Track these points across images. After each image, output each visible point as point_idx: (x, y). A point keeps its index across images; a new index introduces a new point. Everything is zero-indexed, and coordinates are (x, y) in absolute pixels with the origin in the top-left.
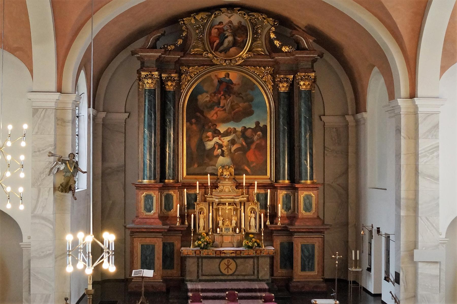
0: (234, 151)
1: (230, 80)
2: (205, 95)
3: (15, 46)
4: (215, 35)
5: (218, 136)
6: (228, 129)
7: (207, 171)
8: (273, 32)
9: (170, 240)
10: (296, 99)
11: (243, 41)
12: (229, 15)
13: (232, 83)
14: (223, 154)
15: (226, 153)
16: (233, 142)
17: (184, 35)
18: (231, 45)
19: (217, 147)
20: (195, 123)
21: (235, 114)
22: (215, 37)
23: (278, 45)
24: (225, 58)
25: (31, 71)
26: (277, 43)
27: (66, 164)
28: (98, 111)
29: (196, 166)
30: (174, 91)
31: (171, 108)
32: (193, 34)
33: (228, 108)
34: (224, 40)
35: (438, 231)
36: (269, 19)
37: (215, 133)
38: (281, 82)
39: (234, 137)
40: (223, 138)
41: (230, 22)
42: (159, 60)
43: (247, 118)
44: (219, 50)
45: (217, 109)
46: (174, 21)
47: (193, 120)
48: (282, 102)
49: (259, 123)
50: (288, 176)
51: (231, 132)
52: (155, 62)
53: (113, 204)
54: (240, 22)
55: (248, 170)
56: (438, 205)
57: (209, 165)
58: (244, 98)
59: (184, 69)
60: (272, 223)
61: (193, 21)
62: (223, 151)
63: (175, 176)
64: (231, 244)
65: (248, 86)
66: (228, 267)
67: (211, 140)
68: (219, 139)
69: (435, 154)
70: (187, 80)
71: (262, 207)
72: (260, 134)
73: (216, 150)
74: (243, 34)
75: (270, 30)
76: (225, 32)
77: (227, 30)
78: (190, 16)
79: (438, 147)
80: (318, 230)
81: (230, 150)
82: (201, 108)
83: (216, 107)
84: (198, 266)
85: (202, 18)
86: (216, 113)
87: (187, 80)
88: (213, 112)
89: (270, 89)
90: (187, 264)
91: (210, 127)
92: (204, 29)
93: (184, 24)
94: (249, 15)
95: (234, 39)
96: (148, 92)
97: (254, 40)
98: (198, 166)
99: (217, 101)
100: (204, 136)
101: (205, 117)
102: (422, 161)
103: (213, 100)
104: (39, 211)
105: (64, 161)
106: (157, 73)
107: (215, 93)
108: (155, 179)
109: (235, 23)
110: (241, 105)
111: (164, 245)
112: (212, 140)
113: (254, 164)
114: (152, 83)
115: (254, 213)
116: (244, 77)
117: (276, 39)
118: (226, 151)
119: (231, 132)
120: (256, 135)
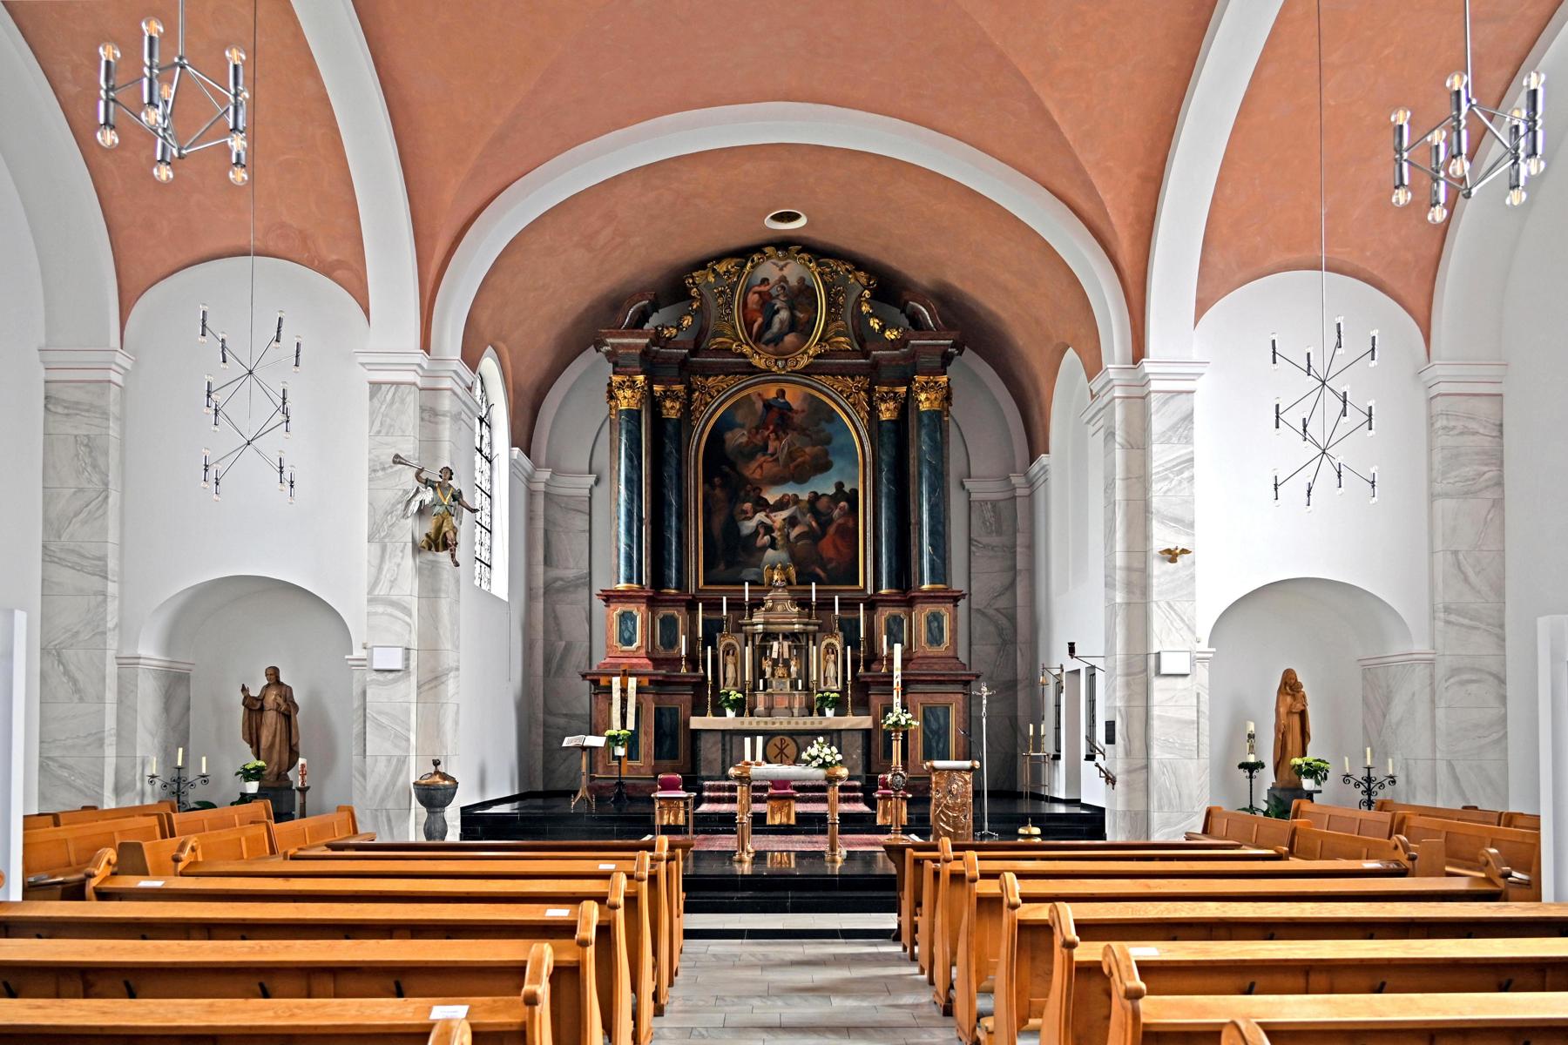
3: (334, 257)
8: (867, 301)
9: (668, 702)
10: (912, 434)
13: (790, 409)
15: (780, 542)
16: (792, 522)
18: (786, 329)
19: (762, 531)
25: (367, 312)
26: (875, 324)
27: (434, 489)
28: (536, 466)
29: (722, 567)
30: (679, 420)
32: (713, 305)
33: (782, 457)
35: (1192, 630)
38: (883, 400)
41: (783, 279)
42: (645, 352)
46: (674, 288)
50: (888, 541)
53: (568, 648)
54: (802, 280)
55: (822, 574)
56: (1193, 578)
60: (867, 668)
61: (711, 279)
62: (773, 539)
63: (681, 585)
66: (782, 750)
69: (1186, 474)
71: (846, 643)
78: (705, 268)
79: (1192, 460)
84: (724, 750)
85: (728, 271)
86: (761, 466)
88: (753, 465)
91: (747, 494)
94: (819, 265)
95: (793, 316)
101: (740, 475)
102: (1158, 489)
104: (382, 590)
105: (428, 483)
106: (641, 377)
107: (757, 428)
108: (640, 581)
109: (793, 281)
110: (807, 450)
111: (659, 712)
116: (813, 397)
117: (872, 315)
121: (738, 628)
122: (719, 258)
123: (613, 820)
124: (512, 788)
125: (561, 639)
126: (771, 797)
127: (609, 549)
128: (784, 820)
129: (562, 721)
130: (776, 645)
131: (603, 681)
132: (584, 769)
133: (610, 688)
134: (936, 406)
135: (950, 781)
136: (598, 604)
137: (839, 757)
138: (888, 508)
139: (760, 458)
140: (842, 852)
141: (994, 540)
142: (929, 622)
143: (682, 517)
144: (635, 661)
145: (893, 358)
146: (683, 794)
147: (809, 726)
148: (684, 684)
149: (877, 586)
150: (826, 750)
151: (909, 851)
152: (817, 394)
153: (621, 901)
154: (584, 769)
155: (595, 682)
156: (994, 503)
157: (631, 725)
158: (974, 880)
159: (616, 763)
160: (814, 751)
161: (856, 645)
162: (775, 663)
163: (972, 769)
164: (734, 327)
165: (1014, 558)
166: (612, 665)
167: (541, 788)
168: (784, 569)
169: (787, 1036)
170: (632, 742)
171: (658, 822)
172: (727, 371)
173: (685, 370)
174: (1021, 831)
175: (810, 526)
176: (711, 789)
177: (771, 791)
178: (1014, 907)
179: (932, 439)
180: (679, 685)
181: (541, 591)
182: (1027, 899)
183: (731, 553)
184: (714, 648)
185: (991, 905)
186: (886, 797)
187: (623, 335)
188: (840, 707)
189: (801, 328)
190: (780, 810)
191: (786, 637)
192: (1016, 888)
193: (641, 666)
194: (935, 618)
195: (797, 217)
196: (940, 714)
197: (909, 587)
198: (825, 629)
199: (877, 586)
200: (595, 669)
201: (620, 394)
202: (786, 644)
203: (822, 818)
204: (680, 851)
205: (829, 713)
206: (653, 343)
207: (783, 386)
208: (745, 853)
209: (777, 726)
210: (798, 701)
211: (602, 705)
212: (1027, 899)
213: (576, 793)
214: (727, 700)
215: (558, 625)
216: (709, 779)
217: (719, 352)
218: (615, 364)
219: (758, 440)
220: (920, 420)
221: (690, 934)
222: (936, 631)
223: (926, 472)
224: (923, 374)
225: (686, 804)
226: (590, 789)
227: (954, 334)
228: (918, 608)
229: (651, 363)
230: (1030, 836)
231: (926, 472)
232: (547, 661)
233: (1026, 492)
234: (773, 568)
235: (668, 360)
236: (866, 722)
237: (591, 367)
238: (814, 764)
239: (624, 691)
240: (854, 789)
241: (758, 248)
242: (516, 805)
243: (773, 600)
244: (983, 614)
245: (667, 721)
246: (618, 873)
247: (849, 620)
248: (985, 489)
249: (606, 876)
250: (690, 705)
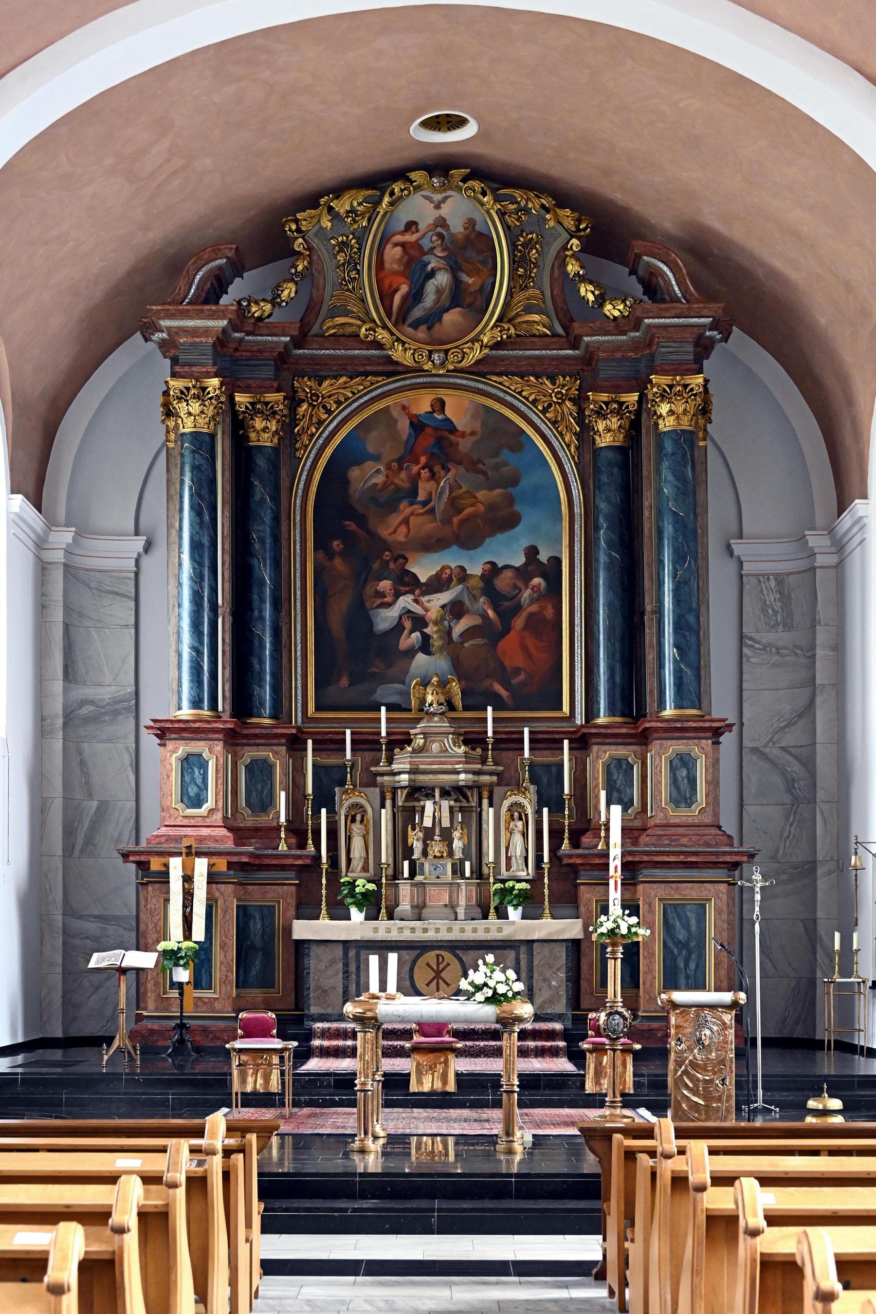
1: (448, 420)
2: (370, 466)
4: (395, 267)
6: (443, 568)
9: (257, 896)
10: (648, 467)
12: (438, 197)
13: (453, 430)
14: (425, 647)
15: (437, 642)
16: (456, 609)
17: (300, 268)
18: (445, 300)
19: (408, 624)
20: (342, 554)
21: (462, 522)
22: (396, 273)
23: (591, 298)
26: (587, 292)
28: (51, 523)
29: (344, 682)
30: (276, 450)
32: (329, 264)
33: (440, 505)
36: (560, 212)
37: (404, 584)
38: (600, 414)
39: (461, 593)
40: (426, 598)
41: (441, 222)
42: (222, 341)
43: (500, 537)
44: (409, 321)
46: (268, 237)
47: (337, 545)
48: (604, 478)
49: (538, 552)
50: (608, 639)
52: (209, 351)
53: (103, 808)
55: (504, 693)
57: (384, 680)
59: (306, 385)
60: (575, 843)
61: (326, 223)
62: (426, 638)
64: (448, 911)
65: (503, 436)
66: (438, 973)
67: (389, 605)
68: (416, 601)
70: (314, 420)
71: (541, 802)
72: (540, 584)
73: (406, 632)
75: (565, 248)
76: (426, 258)
77: (433, 248)
78: (315, 205)
80: (713, 859)
81: (449, 632)
82: (360, 508)
83: (403, 504)
84: (346, 972)
85: (352, 211)
86: (406, 521)
87: (314, 420)
88: (395, 519)
89: (568, 446)
90: (312, 966)
92: (359, 249)
93: (298, 230)
94: (497, 199)
95: (456, 282)
98: (350, 685)
99: (406, 485)
100: (369, 591)
101: (374, 536)
103: (396, 481)
106: (215, 382)
107: (400, 461)
108: (213, 706)
109: (457, 226)
111: (244, 913)
113: (522, 677)
114: (202, 412)
115: (520, 819)
117: (583, 279)
118: (435, 636)
120: (527, 587)
121: (371, 780)
122: (338, 190)
123: (169, 1083)
124: (14, 1032)
125: (90, 796)
126: (417, 1049)
127: (167, 656)
128: (438, 1086)
129: (92, 927)
130: (429, 806)
131: (155, 864)
132: (122, 1004)
133: (166, 874)
134: (686, 424)
135: (700, 1025)
136: (149, 740)
137: (519, 987)
138: (610, 587)
139: (405, 509)
140: (523, 1137)
141: (781, 637)
142: (673, 770)
143: (280, 603)
144: (205, 832)
145: (619, 347)
146: (277, 1044)
147: (481, 936)
148: (283, 868)
149: (591, 712)
150: (498, 976)
151: (617, 1137)
152: (496, 406)
153: (132, 1222)
154: (122, 1004)
155: (143, 866)
156: (780, 579)
157: (199, 933)
158: (701, 1189)
159: (175, 994)
160: (477, 977)
161: (556, 807)
162: (429, 834)
163: (735, 1004)
164: (363, 300)
165: (812, 667)
166: (169, 839)
167: (59, 1034)
168: (443, 684)
170: (201, 961)
171: (236, 1087)
172: (355, 370)
174: (812, 1104)
175: (484, 616)
176: (325, 1034)
177: (417, 1038)
178: (755, 1233)
179: (680, 477)
180: (276, 870)
181: (60, 722)
182: (774, 1219)
183: (358, 659)
184: (331, 812)
185: (723, 1227)
186: (599, 1049)
187: (185, 315)
188: (531, 904)
189: (474, 302)
190: (432, 1068)
191: (445, 793)
192: (756, 1201)
193: (216, 840)
194: (685, 762)
195: (461, 122)
196: (692, 916)
198: (507, 781)
199: (591, 712)
200: (143, 844)
201: (182, 408)
202: (445, 804)
203: (493, 1081)
204: (253, 1138)
205: (514, 914)
206: (234, 326)
207: (442, 393)
208: (372, 1139)
209: (431, 935)
210: (465, 895)
211: (154, 903)
212: (774, 1219)
213: (109, 1040)
214: (352, 894)
215: (86, 775)
216: (322, 1018)
217: (338, 339)
218: (175, 361)
220: (660, 447)
221: (271, 1267)
223: (668, 529)
224: (665, 373)
225: (282, 1058)
226: (133, 1035)
227: (717, 308)
228: (655, 746)
229: (231, 359)
230: (826, 1113)
231: (668, 529)
232: (69, 831)
233: (833, 560)
234: (425, 683)
235: (258, 353)
236: (571, 928)
237: (137, 363)
238: (480, 997)
239: (188, 879)
240: (551, 1035)
241: (401, 174)
242: (20, 1059)
243: (426, 735)
244: (764, 756)
245: (256, 926)
246: (128, 1178)
247: (548, 766)
248: (764, 556)
249: (111, 1179)
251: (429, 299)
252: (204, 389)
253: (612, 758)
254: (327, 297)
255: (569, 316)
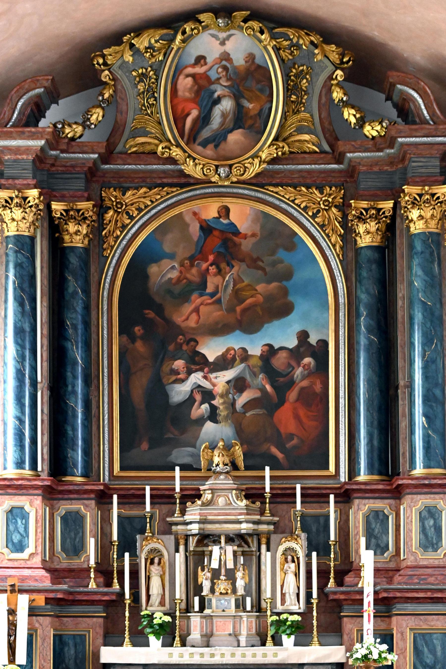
0: (244, 406)
1: (233, 224)
2: (166, 264)
4: (187, 95)
5: (202, 370)
6: (228, 350)
7: (174, 460)
9: (72, 627)
10: (401, 264)
11: (261, 110)
13: (237, 233)
14: (213, 416)
15: (223, 412)
16: (239, 385)
17: (106, 96)
19: (198, 397)
20: (142, 338)
22: (187, 100)
23: (353, 120)
24: (216, 163)
26: (350, 115)
29: (145, 446)
30: (86, 250)
31: (76, 293)
32: (131, 93)
33: (226, 296)
34: (211, 110)
36: (327, 48)
37: (195, 363)
38: (361, 219)
39: (244, 370)
40: (214, 375)
41: (226, 57)
42: (40, 159)
43: (276, 323)
44: (199, 140)
45: (199, 301)
46: (79, 69)
48: (364, 274)
50: (368, 409)
51: (234, 359)
52: (30, 166)
54: (251, 57)
55: (280, 455)
58: (268, 269)
59: (111, 195)
60: (340, 582)
61: (128, 57)
62: (214, 409)
64: (232, 639)
65: (278, 237)
67: (183, 381)
68: (205, 377)
70: (119, 224)
71: (311, 546)
73: (197, 404)
74: (261, 91)
75: (331, 78)
76: (213, 87)
77: (219, 79)
81: (233, 404)
82: (158, 299)
83: (194, 296)
85: (150, 47)
86: (197, 310)
87: (119, 224)
88: (188, 308)
89: (334, 246)
92: (157, 80)
93: (105, 64)
94: (273, 37)
95: (239, 107)
96: (15, 244)
97: (291, 107)
98: (150, 448)
100: (166, 368)
101: (169, 322)
103: (188, 276)
107: (192, 259)
108: (34, 466)
109: (239, 60)
110: (260, 287)
111: (60, 642)
112: (187, 378)
113: (295, 441)
114: (24, 218)
115: (293, 561)
116: (266, 215)
117: (346, 104)
118: (221, 407)
119: (234, 359)
121: (167, 529)
122: (138, 30)
130: (216, 550)
134: (433, 227)
138: (369, 365)
139: (196, 300)
142: (422, 520)
143: (90, 379)
144: (27, 572)
145: (377, 162)
148: (92, 603)
149: (353, 471)
162: (216, 574)
164: (160, 123)
168: (228, 448)
169: (24, 379)
172: (153, 182)
173: (95, 180)
175: (263, 390)
179: (428, 272)
183: (156, 427)
188: (302, 632)
189: (250, 122)
191: (230, 540)
194: (431, 515)
197: (396, 473)
198: (283, 529)
199: (353, 471)
202: (230, 549)
205: (288, 641)
207: (227, 201)
210: (247, 624)
214: (150, 625)
219: (193, 274)
220: (411, 247)
222: (431, 532)
223: (418, 316)
224: (415, 184)
228: (407, 500)
229: (48, 173)
231: (418, 316)
234: (213, 447)
235: (71, 168)
243: (213, 491)
245: (70, 652)
247: (316, 517)
250: (101, 631)
251: (216, 121)
252: (25, 199)
253: (371, 511)
254: (130, 119)
255: (334, 135)
